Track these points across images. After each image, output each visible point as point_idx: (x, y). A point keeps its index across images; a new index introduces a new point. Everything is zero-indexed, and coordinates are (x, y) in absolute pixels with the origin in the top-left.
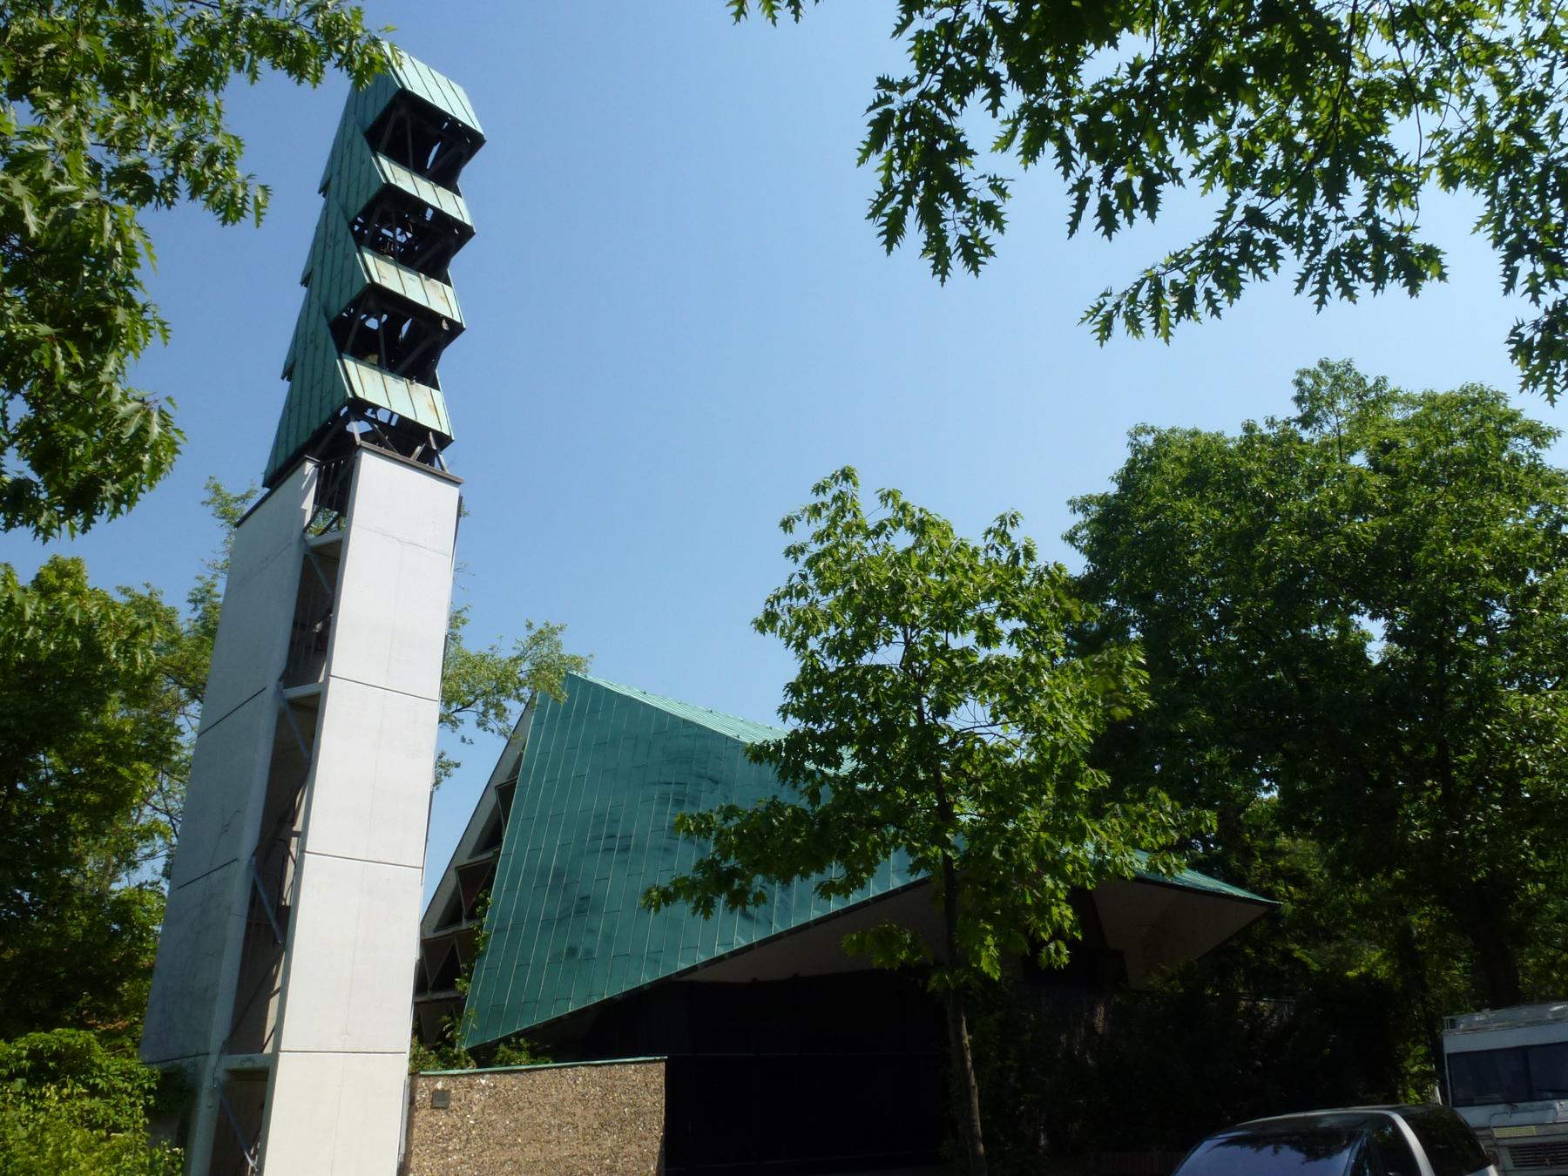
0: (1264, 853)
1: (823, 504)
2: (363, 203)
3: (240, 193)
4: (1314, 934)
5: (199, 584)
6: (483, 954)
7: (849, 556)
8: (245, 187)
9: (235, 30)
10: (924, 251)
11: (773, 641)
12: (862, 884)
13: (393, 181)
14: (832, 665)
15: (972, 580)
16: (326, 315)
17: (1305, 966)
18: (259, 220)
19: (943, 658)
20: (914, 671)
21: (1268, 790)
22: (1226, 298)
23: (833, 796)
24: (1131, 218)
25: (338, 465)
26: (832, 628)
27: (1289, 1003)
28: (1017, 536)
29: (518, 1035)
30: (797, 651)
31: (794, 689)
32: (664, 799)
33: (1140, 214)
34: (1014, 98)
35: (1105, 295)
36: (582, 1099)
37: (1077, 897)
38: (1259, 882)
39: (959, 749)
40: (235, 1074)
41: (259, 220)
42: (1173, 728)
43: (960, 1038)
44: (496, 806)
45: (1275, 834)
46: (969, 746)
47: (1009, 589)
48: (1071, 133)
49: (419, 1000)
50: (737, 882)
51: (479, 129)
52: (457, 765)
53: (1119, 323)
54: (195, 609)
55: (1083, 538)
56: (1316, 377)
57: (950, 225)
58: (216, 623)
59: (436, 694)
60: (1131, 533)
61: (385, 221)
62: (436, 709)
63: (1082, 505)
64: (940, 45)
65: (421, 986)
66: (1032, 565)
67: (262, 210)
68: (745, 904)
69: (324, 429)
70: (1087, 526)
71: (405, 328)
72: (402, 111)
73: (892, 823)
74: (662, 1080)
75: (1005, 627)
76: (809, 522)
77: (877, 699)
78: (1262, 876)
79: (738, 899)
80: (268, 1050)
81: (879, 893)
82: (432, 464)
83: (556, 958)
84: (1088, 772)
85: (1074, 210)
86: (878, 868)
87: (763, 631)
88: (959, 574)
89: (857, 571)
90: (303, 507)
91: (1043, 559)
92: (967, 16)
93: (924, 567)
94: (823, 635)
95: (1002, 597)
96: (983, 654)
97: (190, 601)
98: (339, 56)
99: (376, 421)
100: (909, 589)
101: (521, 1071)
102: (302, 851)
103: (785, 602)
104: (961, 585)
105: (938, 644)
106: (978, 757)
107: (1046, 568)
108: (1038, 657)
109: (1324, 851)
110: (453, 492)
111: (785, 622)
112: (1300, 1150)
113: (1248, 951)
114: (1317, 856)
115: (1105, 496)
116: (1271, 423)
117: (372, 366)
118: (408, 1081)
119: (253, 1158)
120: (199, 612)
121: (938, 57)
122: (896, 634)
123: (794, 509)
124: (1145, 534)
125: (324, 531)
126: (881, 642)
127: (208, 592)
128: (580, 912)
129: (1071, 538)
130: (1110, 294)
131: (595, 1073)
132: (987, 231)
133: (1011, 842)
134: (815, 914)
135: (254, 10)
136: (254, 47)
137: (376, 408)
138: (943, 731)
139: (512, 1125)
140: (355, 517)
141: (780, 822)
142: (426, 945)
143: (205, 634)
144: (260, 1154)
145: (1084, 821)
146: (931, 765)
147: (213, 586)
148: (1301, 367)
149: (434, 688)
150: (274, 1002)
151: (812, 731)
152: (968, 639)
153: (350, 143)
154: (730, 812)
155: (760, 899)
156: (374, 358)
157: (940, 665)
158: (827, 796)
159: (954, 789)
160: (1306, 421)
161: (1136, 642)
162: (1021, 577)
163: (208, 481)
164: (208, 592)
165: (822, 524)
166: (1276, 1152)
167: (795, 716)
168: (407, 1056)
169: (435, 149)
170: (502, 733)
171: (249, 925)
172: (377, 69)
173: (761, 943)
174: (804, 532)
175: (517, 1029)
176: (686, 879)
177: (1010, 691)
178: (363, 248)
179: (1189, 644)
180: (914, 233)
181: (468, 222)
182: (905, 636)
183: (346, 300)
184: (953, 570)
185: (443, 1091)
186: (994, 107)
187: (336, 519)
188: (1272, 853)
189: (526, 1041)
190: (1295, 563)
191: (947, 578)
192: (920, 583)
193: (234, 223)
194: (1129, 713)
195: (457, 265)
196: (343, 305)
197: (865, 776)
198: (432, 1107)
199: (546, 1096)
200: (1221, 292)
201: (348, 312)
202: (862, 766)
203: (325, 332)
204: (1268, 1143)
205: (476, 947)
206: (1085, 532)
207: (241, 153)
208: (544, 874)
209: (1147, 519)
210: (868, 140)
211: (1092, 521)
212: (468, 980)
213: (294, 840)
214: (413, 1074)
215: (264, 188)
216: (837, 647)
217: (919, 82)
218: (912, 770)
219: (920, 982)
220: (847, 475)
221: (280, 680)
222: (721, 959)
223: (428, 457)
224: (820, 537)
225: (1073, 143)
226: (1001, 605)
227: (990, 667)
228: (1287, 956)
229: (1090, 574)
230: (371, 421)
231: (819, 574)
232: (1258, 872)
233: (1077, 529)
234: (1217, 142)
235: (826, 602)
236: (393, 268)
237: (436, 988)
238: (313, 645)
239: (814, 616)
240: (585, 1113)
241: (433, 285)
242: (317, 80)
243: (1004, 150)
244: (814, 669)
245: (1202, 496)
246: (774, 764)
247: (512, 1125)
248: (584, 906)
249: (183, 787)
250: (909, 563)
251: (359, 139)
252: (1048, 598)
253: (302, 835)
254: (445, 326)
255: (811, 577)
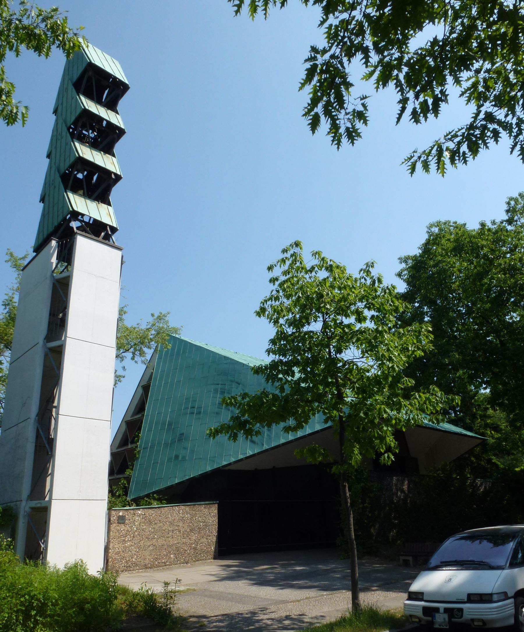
0: (481, 416)
1: (286, 258)
2: (73, 118)
3: (15, 111)
4: (501, 451)
5: (6, 297)
6: (138, 458)
7: (298, 281)
8: (17, 108)
9: (9, 30)
10: (329, 133)
11: (264, 320)
12: (302, 427)
13: (87, 108)
14: (290, 330)
15: (353, 293)
16: (59, 171)
17: (497, 466)
18: (24, 123)
19: (340, 328)
20: (327, 334)
21: (485, 388)
22: (472, 156)
23: (290, 389)
24: (426, 118)
25: (66, 241)
26: (290, 314)
27: (489, 482)
28: (374, 272)
29: (154, 493)
30: (274, 325)
31: (273, 342)
32: (216, 391)
33: (431, 116)
34: (374, 58)
35: (414, 152)
36: (182, 519)
37: (398, 434)
38: (479, 429)
39: (346, 369)
40: (33, 509)
41: (24, 123)
42: (444, 362)
43: (345, 493)
44: (142, 394)
45: (486, 409)
46: (351, 367)
47: (371, 297)
48: (401, 77)
49: (111, 478)
50: (248, 426)
51: (127, 82)
52: (124, 377)
53: (419, 166)
54: (5, 309)
55: (405, 275)
56: (516, 200)
57: (342, 122)
58: (15, 315)
59: (114, 344)
60: (427, 273)
61: (84, 127)
62: (113, 352)
63: (405, 260)
64: (341, 32)
65: (111, 472)
66: (381, 286)
67: (25, 119)
68: (251, 436)
69: (59, 226)
70: (407, 269)
71: (95, 178)
72: (90, 73)
73: (317, 401)
74: (216, 511)
75: (368, 313)
76: (280, 266)
77: (310, 346)
78: (480, 426)
79: (249, 433)
80: (47, 499)
81: (310, 432)
82: (109, 241)
83: (169, 460)
84: (404, 379)
85: (399, 112)
86: (310, 421)
87: (260, 316)
88: (348, 290)
89: (301, 288)
90: (52, 261)
91: (386, 283)
92: (354, 17)
93: (332, 287)
94: (286, 318)
95: (367, 300)
96: (358, 326)
97: (3, 305)
98: (59, 43)
99: (83, 221)
100: (325, 297)
101: (156, 508)
102: (58, 414)
103: (269, 303)
104: (348, 294)
105: (338, 322)
106: (355, 372)
107: (388, 287)
108: (383, 327)
109: (508, 416)
110: (119, 253)
111: (269, 312)
112: (491, 542)
113: (473, 459)
114: (505, 418)
115: (415, 256)
116: (494, 223)
117: (80, 195)
118: (107, 512)
119: (43, 543)
120: (7, 310)
121: (340, 38)
122: (319, 317)
123: (273, 261)
124: (433, 274)
125: (61, 272)
126: (313, 320)
127: (11, 301)
128: (180, 440)
129: (399, 275)
130: (416, 152)
131: (187, 508)
132: (359, 125)
133: (368, 409)
134: (282, 441)
135: (17, 19)
136: (18, 39)
137: (83, 215)
138: (340, 361)
139: (152, 530)
140: (75, 265)
141: (267, 400)
142: (113, 455)
143: (10, 319)
144: (46, 543)
145: (402, 400)
146: (334, 376)
147: (13, 298)
148: (509, 196)
149: (113, 342)
150: (48, 479)
151: (281, 360)
152: (352, 320)
153: (67, 89)
154: (245, 395)
155: (258, 433)
156: (81, 192)
157: (339, 331)
158: (288, 389)
159: (344, 386)
160: (510, 221)
161: (427, 322)
162: (376, 291)
163: (7, 251)
164: (11, 301)
165: (286, 267)
166: (480, 543)
167: (273, 354)
168: (106, 501)
169: (106, 92)
170: (143, 362)
171: (36, 446)
172: (76, 49)
173: (259, 453)
174: (277, 272)
175: (154, 490)
176: (226, 424)
177: (370, 342)
178: (74, 140)
179: (451, 323)
180: (325, 124)
181: (122, 127)
182: (323, 318)
183: (67, 165)
184: (345, 288)
185: (122, 516)
186: (366, 63)
187: (67, 267)
188: (484, 417)
189: (157, 495)
190: (501, 288)
191: (342, 292)
192: (330, 294)
193: (12, 125)
194: (423, 354)
195: (118, 147)
196: (65, 169)
197: (305, 380)
198: (118, 523)
199: (167, 518)
200: (469, 154)
201: (68, 170)
202: (303, 376)
203: (58, 180)
204: (477, 539)
205: (135, 455)
206: (406, 272)
207: (14, 91)
208: (164, 424)
209: (434, 266)
210: (304, 78)
211: (409, 267)
212: (132, 470)
213: (54, 410)
214: (109, 509)
215: (26, 107)
216: (292, 323)
217: (329, 50)
218: (325, 378)
219: (328, 470)
220: (297, 244)
221: (45, 339)
222: (241, 460)
223: (107, 238)
224: (285, 273)
225: (403, 83)
226: (366, 304)
227: (361, 332)
228: (489, 461)
229: (408, 292)
230: (81, 221)
231: (284, 290)
232: (478, 425)
233: (402, 271)
234: (473, 80)
235: (287, 303)
236: (88, 149)
237: (119, 473)
238: (59, 323)
239: (282, 308)
240: (183, 525)
241: (107, 157)
242: (47, 55)
243: (367, 80)
244: (282, 333)
245: (461, 256)
246: (263, 375)
247: (152, 530)
248: (182, 438)
249: (4, 388)
250: (325, 285)
251: (71, 87)
252: (388, 301)
253: (57, 407)
254: (113, 176)
255: (281, 291)
